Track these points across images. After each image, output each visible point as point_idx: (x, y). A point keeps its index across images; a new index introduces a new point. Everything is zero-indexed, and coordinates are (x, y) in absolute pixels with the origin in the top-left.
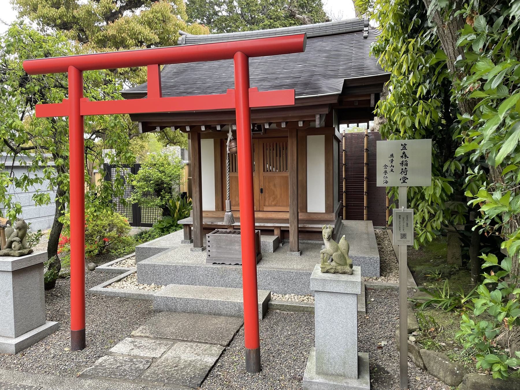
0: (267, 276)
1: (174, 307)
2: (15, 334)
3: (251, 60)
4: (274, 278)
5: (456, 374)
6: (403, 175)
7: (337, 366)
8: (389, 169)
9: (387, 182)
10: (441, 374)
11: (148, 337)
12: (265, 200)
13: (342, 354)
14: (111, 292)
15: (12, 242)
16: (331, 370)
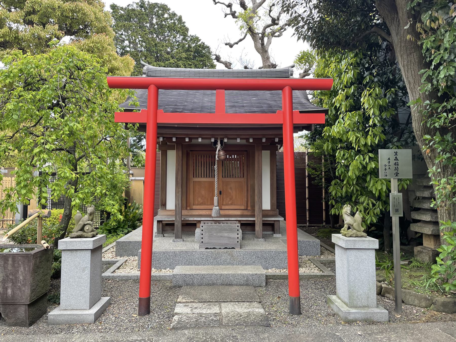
0: (252, 256)
1: (191, 282)
5: (429, 300)
6: (396, 171)
7: (363, 301)
8: (387, 168)
10: (416, 302)
11: (193, 302)
12: (223, 200)
13: (367, 292)
14: (124, 276)
15: (85, 225)
16: (359, 304)
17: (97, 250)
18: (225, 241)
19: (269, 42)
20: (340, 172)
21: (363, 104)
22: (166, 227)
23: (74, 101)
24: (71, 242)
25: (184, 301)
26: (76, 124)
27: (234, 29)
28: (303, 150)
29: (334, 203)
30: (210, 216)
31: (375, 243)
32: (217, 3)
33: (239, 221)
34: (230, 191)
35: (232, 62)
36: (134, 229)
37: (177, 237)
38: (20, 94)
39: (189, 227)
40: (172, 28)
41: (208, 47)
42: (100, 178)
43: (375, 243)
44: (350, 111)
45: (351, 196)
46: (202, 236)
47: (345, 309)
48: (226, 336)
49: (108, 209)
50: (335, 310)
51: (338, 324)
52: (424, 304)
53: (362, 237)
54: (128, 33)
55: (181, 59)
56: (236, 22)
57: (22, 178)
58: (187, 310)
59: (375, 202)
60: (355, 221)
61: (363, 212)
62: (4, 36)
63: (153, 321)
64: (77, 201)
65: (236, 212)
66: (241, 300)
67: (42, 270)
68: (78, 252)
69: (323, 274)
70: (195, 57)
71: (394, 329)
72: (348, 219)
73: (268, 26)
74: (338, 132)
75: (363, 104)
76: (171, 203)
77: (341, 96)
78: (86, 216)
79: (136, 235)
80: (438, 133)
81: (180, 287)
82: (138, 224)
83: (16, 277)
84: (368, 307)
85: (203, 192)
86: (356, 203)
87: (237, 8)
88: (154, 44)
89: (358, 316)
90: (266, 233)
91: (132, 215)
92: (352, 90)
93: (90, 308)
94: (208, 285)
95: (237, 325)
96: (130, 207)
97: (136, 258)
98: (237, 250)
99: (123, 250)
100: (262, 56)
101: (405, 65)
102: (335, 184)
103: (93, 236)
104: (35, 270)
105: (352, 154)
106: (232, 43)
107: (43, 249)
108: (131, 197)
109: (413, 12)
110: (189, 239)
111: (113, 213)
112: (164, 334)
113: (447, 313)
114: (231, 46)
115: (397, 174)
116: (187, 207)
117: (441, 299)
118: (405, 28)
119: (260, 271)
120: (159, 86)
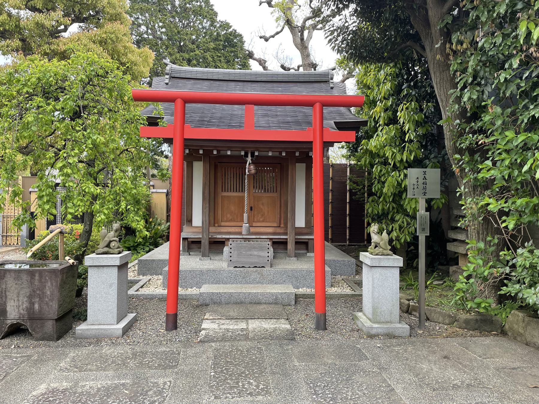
2: (117, 321)
4: (289, 276)
5: (452, 317)
8: (416, 187)
10: (441, 319)
12: (254, 217)
15: (111, 241)
16: (382, 320)
17: (123, 267)
18: (255, 260)
19: (310, 37)
20: (376, 188)
21: (400, 118)
22: (193, 245)
23: (96, 112)
24: (97, 258)
25: (211, 318)
26: (99, 136)
27: (268, 19)
28: (344, 161)
29: (370, 221)
30: (240, 233)
31: (399, 261)
33: (270, 239)
34: (261, 207)
35: (266, 60)
36: (157, 247)
37: (203, 256)
38: (40, 105)
39: (216, 245)
40: (198, 12)
41: (241, 35)
42: (123, 193)
43: (399, 261)
44: (388, 125)
45: (388, 214)
46: (230, 254)
47: (368, 324)
48: (251, 348)
49: (134, 225)
50: (360, 325)
51: (360, 338)
52: (447, 321)
53: (388, 255)
54: (145, 17)
55: (208, 50)
56: (272, 13)
57: (44, 193)
58: (214, 326)
59: (409, 220)
60: (382, 240)
61: (398, 231)
62: (3, 24)
63: (181, 335)
64: (103, 217)
65: (269, 229)
67: (68, 286)
68: (105, 268)
69: (354, 293)
70: (225, 47)
71: (413, 343)
72: (375, 238)
73: (309, 19)
74: (375, 146)
75: (400, 118)
76: (197, 219)
77: (380, 106)
78: (112, 233)
79: (162, 252)
80: (467, 153)
81: (207, 305)
82: (161, 241)
83: (43, 293)
84: (391, 322)
85: (233, 208)
86: (393, 220)
88: (176, 31)
89: (380, 331)
90: (299, 252)
91: (153, 231)
92: (390, 103)
93: (117, 323)
94: (236, 303)
95: (263, 338)
96: (151, 223)
97: (161, 277)
98: (268, 268)
99: (147, 268)
101: (438, 83)
102: (373, 201)
103: (120, 253)
104: (62, 285)
105: (389, 169)
106: (268, 35)
107: (68, 265)
108: (152, 212)
109: (445, 30)
110: (217, 258)
111: (139, 229)
112: (191, 346)
113: (469, 330)
114: (267, 40)
116: (214, 223)
117: (463, 316)
118: (436, 46)
119: (289, 289)
120: (187, 100)
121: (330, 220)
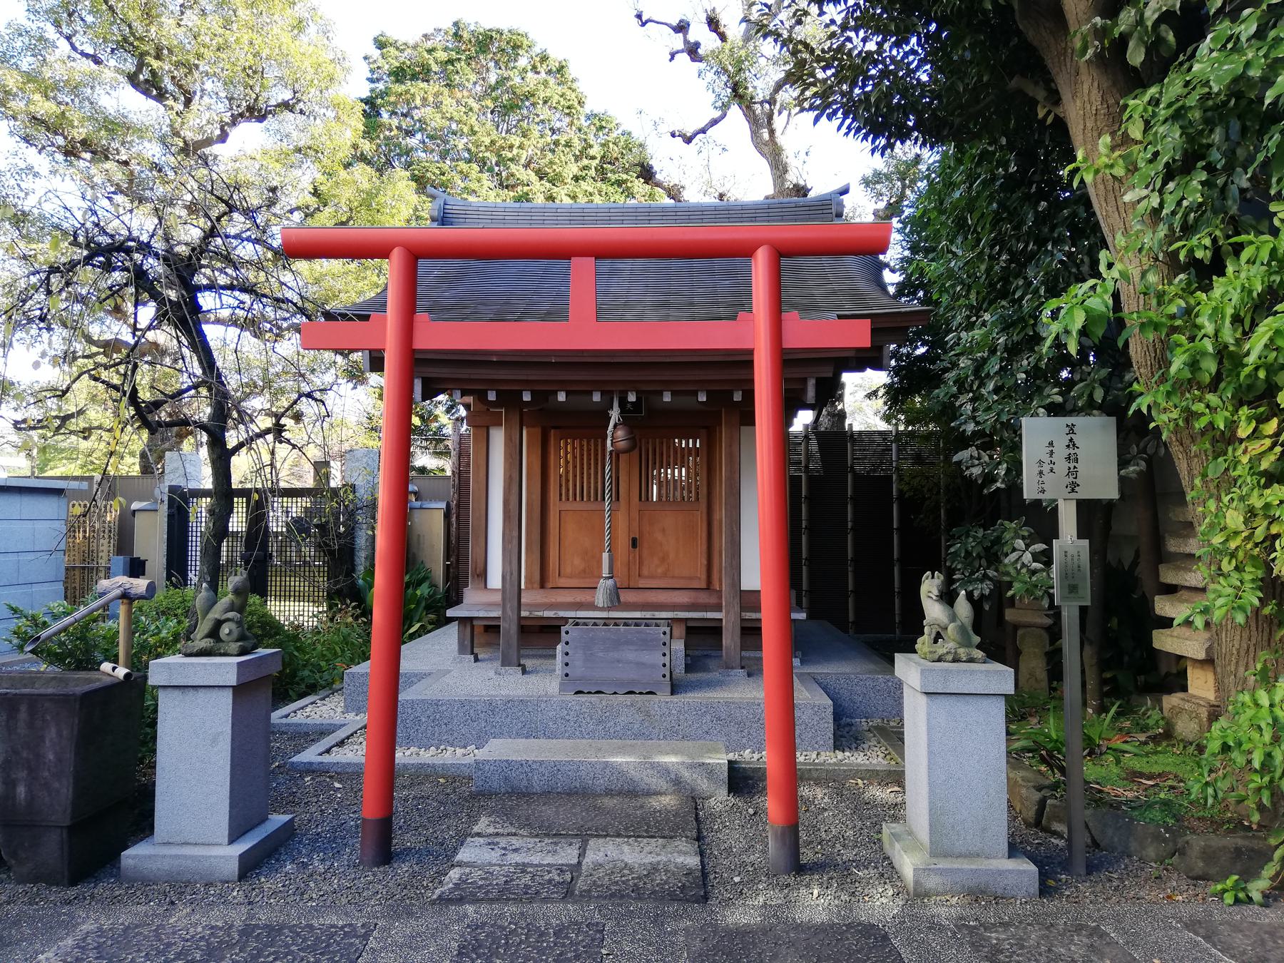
1: (525, 783)
2: (230, 835)
3: (421, 262)
6: (1071, 479)
8: (1046, 468)
9: (1043, 491)
11: (515, 834)
25: (491, 830)
30: (592, 606)
32: (647, 22)
34: (659, 536)
37: (506, 662)
39: (540, 635)
66: (646, 831)
68: (201, 693)
72: (934, 610)
87: (699, 32)
95: (613, 895)
100: (771, 165)
114: (688, 140)
115: (1073, 487)
121: (850, 575)
